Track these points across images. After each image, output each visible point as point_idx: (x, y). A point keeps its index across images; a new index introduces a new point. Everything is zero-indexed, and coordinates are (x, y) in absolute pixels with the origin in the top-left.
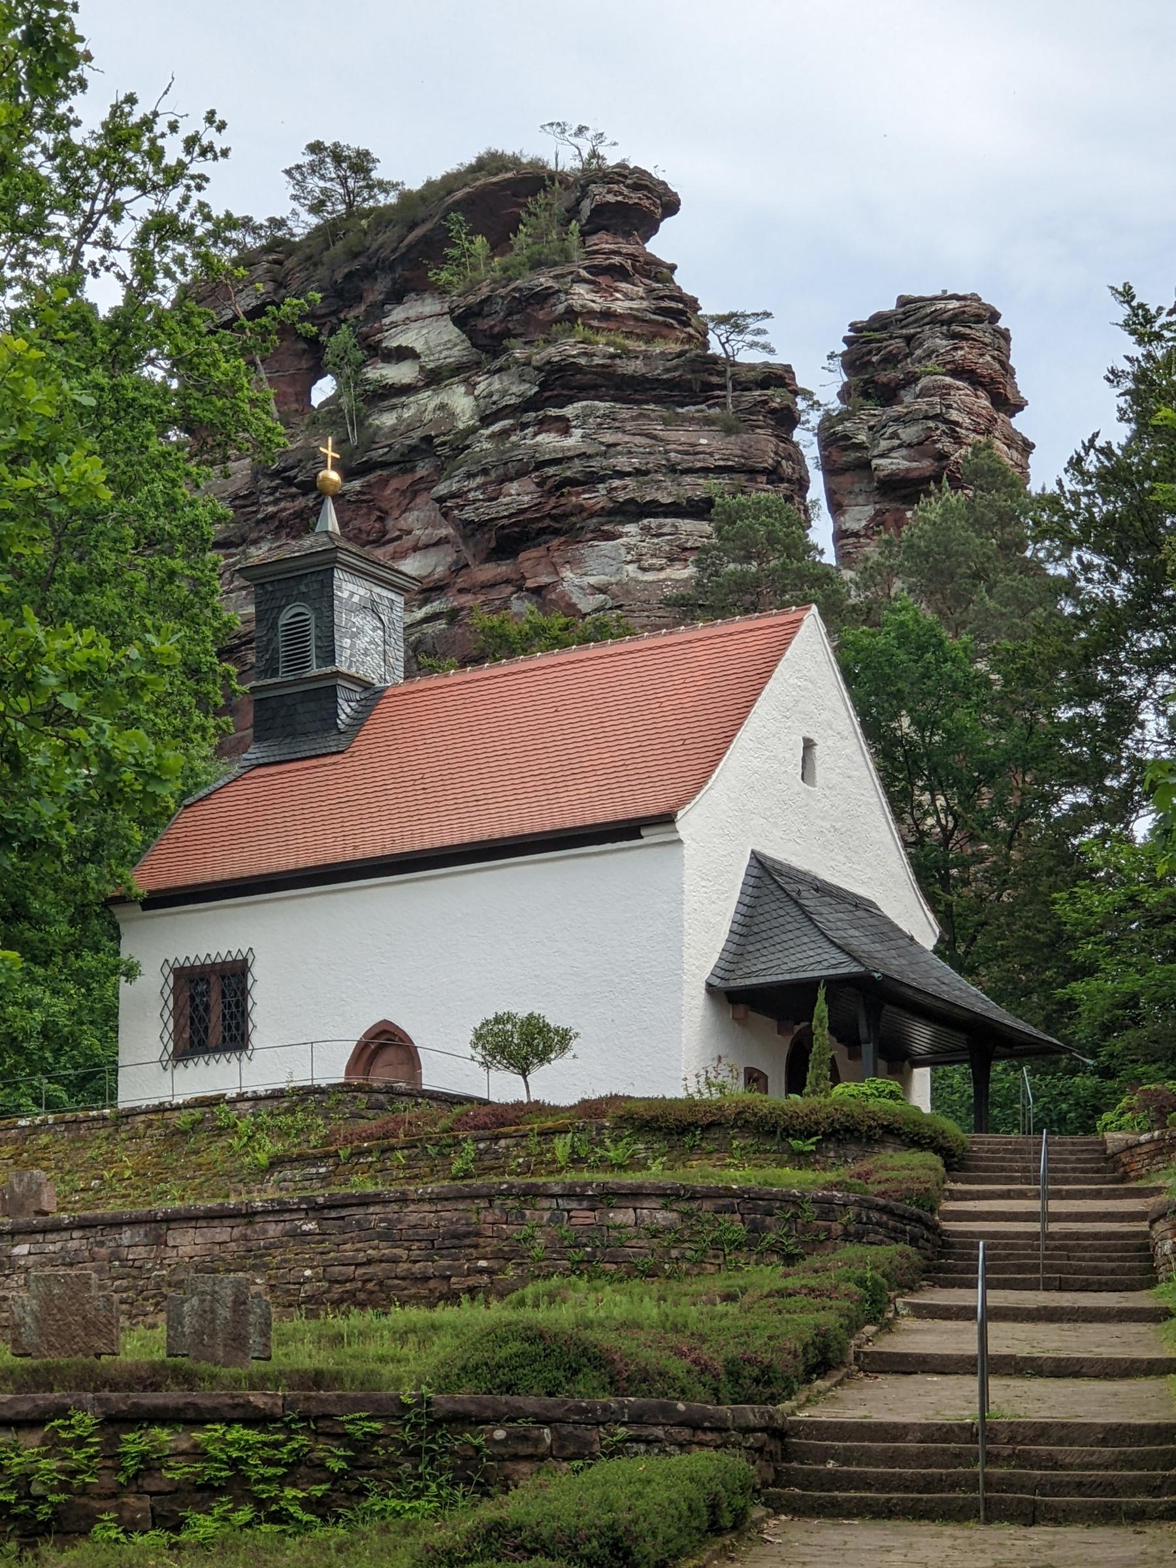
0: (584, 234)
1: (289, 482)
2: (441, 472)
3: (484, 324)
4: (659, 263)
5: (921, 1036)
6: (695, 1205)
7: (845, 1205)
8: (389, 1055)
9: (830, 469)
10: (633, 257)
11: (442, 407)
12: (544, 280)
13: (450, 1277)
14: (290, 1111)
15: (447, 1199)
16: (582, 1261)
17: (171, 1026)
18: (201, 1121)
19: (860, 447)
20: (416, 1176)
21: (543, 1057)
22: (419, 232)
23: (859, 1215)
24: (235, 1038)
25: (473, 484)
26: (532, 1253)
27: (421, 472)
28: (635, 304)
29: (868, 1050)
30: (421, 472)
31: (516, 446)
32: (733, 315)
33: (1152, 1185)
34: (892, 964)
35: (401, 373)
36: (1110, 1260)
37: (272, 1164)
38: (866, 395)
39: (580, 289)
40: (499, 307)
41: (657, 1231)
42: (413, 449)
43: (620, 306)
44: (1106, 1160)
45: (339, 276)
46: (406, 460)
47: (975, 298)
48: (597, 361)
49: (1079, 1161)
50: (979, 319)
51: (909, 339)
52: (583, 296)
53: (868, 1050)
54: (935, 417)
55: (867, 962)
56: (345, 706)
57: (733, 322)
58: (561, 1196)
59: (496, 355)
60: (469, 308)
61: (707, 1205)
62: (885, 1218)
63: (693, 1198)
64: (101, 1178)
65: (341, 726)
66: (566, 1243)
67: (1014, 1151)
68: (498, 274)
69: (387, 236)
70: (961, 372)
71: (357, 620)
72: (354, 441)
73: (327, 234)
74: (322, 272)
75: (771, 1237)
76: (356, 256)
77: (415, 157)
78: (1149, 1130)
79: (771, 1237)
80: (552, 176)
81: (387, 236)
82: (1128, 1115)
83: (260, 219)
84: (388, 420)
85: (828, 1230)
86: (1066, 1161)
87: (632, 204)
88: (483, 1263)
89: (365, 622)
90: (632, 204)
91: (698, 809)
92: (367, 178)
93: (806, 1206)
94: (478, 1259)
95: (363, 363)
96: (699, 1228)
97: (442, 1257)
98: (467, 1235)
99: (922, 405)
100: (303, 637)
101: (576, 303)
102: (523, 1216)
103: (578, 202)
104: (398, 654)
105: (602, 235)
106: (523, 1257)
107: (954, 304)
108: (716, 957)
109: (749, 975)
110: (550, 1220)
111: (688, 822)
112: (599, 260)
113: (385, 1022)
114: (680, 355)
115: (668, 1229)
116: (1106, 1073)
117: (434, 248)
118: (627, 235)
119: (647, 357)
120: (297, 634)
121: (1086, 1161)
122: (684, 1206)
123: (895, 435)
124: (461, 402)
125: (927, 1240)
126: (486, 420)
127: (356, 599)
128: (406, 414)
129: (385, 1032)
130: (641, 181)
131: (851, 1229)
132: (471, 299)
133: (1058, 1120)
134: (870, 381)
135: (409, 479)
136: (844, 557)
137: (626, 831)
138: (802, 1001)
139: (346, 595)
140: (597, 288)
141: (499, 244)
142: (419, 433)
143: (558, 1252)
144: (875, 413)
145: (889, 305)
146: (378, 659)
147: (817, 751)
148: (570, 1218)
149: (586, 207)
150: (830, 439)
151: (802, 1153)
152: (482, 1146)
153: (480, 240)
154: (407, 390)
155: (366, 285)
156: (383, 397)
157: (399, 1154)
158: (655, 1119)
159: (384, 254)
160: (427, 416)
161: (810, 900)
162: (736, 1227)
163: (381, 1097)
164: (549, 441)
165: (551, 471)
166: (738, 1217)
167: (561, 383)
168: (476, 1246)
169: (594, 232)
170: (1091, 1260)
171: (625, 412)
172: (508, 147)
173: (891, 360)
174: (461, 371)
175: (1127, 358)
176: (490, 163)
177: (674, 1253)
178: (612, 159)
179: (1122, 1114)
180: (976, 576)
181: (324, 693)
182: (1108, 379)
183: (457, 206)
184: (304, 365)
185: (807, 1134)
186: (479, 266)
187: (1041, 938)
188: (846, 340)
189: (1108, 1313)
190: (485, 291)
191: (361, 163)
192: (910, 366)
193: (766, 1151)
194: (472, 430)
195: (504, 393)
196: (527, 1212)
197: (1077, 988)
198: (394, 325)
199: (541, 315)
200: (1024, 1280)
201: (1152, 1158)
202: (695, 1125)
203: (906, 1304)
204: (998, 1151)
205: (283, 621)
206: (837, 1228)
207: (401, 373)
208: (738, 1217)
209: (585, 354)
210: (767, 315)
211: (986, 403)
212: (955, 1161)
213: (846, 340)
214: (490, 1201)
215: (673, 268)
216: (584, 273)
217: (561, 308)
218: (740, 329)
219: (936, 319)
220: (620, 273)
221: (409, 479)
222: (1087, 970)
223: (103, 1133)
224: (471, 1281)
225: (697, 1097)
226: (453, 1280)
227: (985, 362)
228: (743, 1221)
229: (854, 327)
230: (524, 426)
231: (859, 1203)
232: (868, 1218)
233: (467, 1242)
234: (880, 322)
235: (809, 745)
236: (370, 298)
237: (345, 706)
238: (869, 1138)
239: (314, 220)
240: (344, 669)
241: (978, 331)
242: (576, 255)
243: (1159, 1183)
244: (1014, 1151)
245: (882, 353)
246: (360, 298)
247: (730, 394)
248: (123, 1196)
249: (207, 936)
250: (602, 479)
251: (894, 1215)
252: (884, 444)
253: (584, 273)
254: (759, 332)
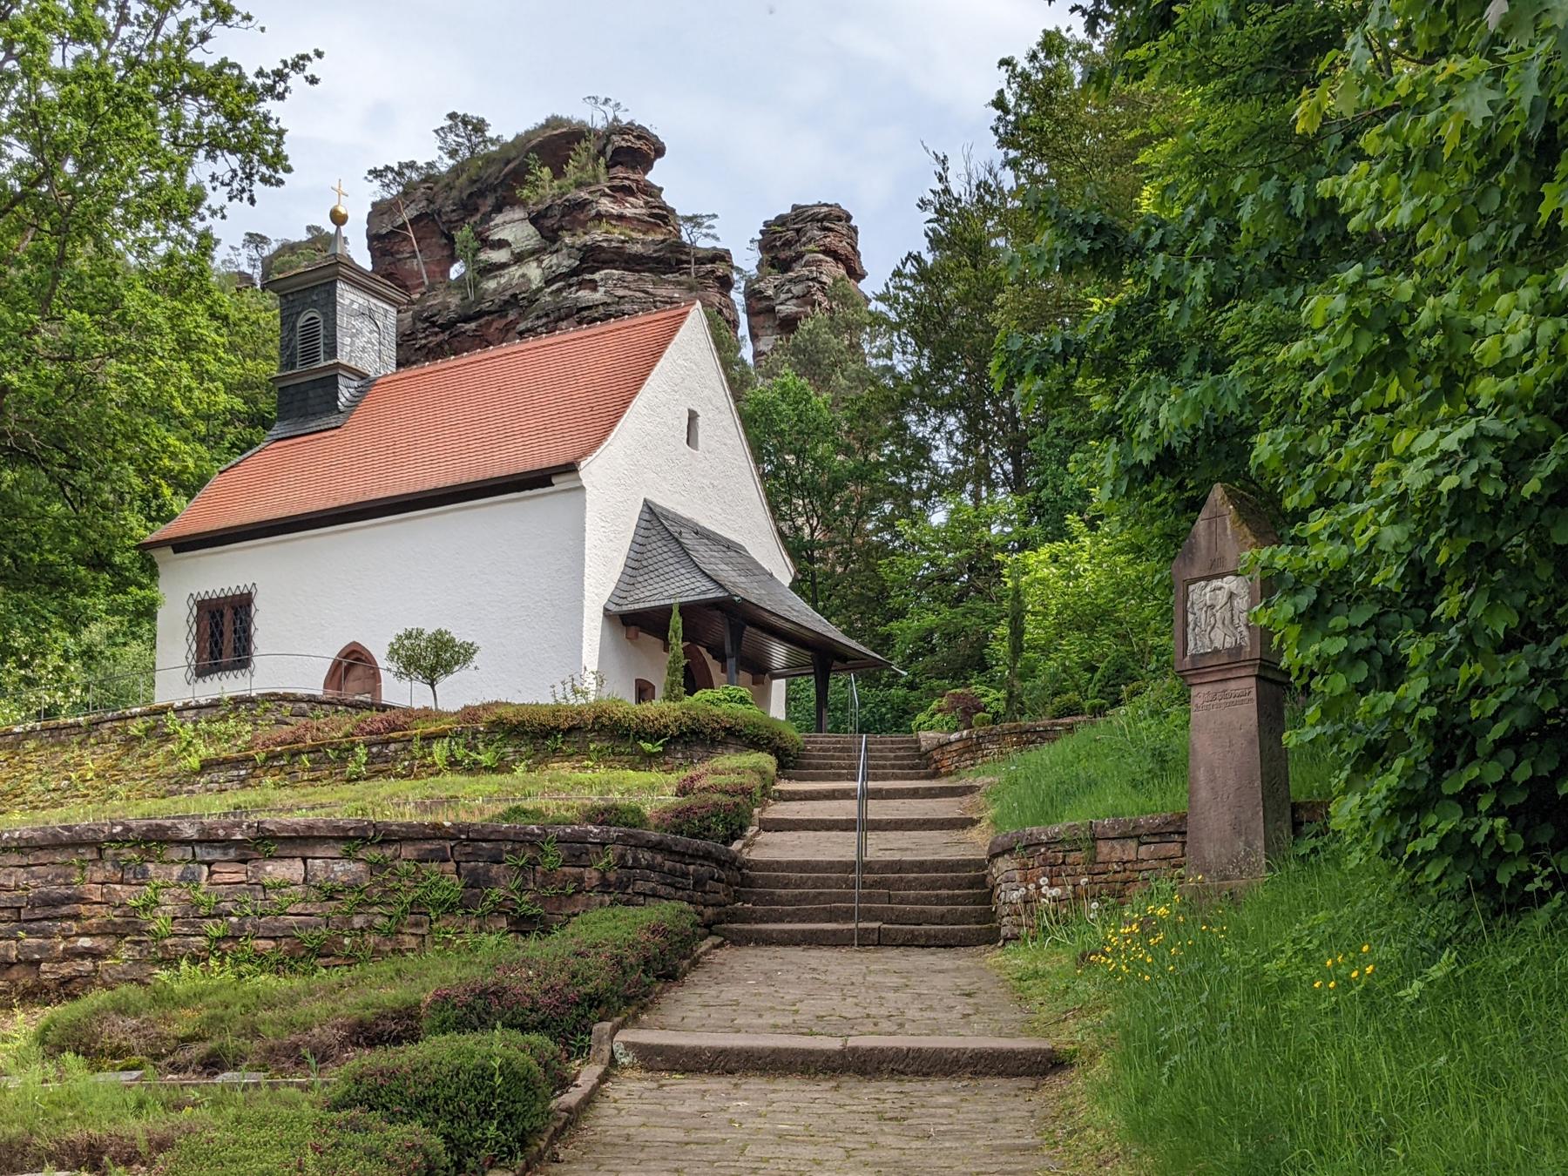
0: (608, 167)
1: (434, 324)
2: (523, 316)
3: (548, 223)
4: (653, 186)
5: (779, 654)
6: (389, 852)
7: (603, 845)
8: (358, 671)
9: (750, 313)
10: (637, 181)
11: (523, 276)
12: (584, 195)
13: (39, 962)
14: (224, 719)
15: (41, 848)
16: (224, 938)
17: (194, 647)
18: (154, 728)
19: (769, 298)
20: (317, 779)
21: (448, 668)
22: (511, 166)
23: (622, 856)
24: (241, 659)
25: (540, 323)
26: (153, 927)
27: (511, 317)
29: (731, 662)
30: (511, 317)
31: (566, 298)
32: (695, 217)
33: (961, 783)
35: (500, 256)
36: (940, 901)
37: (202, 767)
38: (773, 266)
39: (604, 200)
40: (557, 212)
41: (334, 890)
42: (506, 302)
44: (920, 757)
45: (464, 196)
46: (502, 310)
47: (837, 206)
49: (896, 758)
50: (839, 219)
51: (798, 231)
52: (606, 205)
53: (731, 662)
54: (813, 279)
55: (729, 586)
56: (345, 391)
57: (695, 220)
58: (199, 842)
59: (554, 242)
60: (539, 212)
61: (408, 851)
62: (659, 858)
63: (385, 842)
64: (69, 779)
65: (341, 408)
66: (202, 911)
67: (842, 750)
68: (556, 191)
69: (492, 169)
70: (828, 252)
71: (357, 323)
72: (472, 298)
73: (456, 171)
74: (455, 193)
75: (497, 893)
76: (475, 182)
77: (509, 123)
78: (956, 729)
79: (497, 893)
80: (589, 131)
81: (492, 169)
82: (939, 716)
83: (421, 163)
84: (491, 285)
85: (580, 880)
86: (885, 758)
87: (633, 151)
88: (85, 942)
89: (366, 326)
90: (633, 151)
91: (598, 461)
92: (483, 135)
93: (547, 848)
94: (78, 935)
95: (479, 250)
96: (395, 884)
97: (29, 933)
98: (66, 900)
99: (805, 271)
100: (315, 336)
101: (602, 208)
102: (145, 872)
103: (605, 146)
104: (391, 354)
105: (619, 168)
106: (140, 933)
107: (825, 209)
108: (613, 586)
109: (637, 601)
110: (182, 878)
111: (590, 471)
112: (617, 182)
113: (355, 643)
114: (663, 241)
115: (350, 887)
116: (912, 686)
117: (519, 175)
118: (634, 168)
119: (644, 243)
120: (310, 332)
121: (903, 758)
122: (373, 854)
123: (789, 291)
124: (534, 272)
125: (720, 880)
126: (548, 282)
127: (355, 306)
128: (503, 281)
129: (353, 652)
130: (642, 134)
131: (612, 876)
132: (540, 207)
135: (504, 322)
136: (757, 365)
137: (538, 479)
138: (693, 630)
139: (347, 302)
140: (615, 201)
141: (558, 173)
142: (510, 292)
143: (192, 925)
144: (775, 278)
145: (786, 210)
146: (374, 356)
147: (700, 421)
148: (211, 874)
149: (609, 149)
150: (752, 294)
151: (652, 755)
152: (374, 750)
153: (546, 170)
154: (504, 266)
155: (480, 201)
156: (490, 271)
157: (304, 757)
158: (522, 723)
159: (491, 180)
160: (514, 282)
161: (688, 540)
162: (447, 879)
163: (304, 705)
164: (585, 295)
166: (451, 866)
167: (592, 258)
168: (76, 917)
169: (614, 166)
170: (917, 901)
171: (629, 276)
172: (564, 114)
173: (788, 244)
174: (535, 253)
176: (554, 122)
177: (358, 921)
178: (625, 119)
179: (933, 715)
180: (834, 364)
181: (328, 384)
183: (533, 149)
184: (446, 253)
185: (654, 737)
186: (545, 187)
187: (871, 594)
188: (762, 232)
189: (956, 1060)
190: (549, 202)
191: (479, 127)
193: (622, 753)
194: (540, 290)
195: (559, 266)
196: (151, 866)
198: (497, 226)
199: (582, 217)
200: (834, 932)
201: (961, 755)
202: (556, 729)
203: (629, 1046)
204: (828, 750)
205: (300, 324)
206: (591, 876)
207: (500, 256)
208: (451, 866)
211: (843, 272)
212: (790, 762)
213: (762, 232)
214: (100, 851)
215: (661, 189)
217: (593, 212)
218: (699, 225)
219: (814, 218)
220: (628, 191)
221: (504, 322)
222: (900, 614)
223: (76, 739)
224: (66, 970)
225: (564, 702)
226: (44, 967)
227: (843, 247)
228: (458, 873)
229: (766, 224)
230: (571, 286)
231: (623, 840)
232: (635, 859)
233: (64, 910)
234: (781, 220)
235: (693, 416)
236: (483, 209)
237: (345, 391)
238: (713, 740)
239: (451, 162)
240: (344, 362)
242: (603, 178)
243: (970, 781)
244: (842, 750)
246: (477, 210)
247: (693, 267)
248: (85, 796)
249: (218, 575)
251: (671, 852)
252: (783, 296)
254: (710, 227)
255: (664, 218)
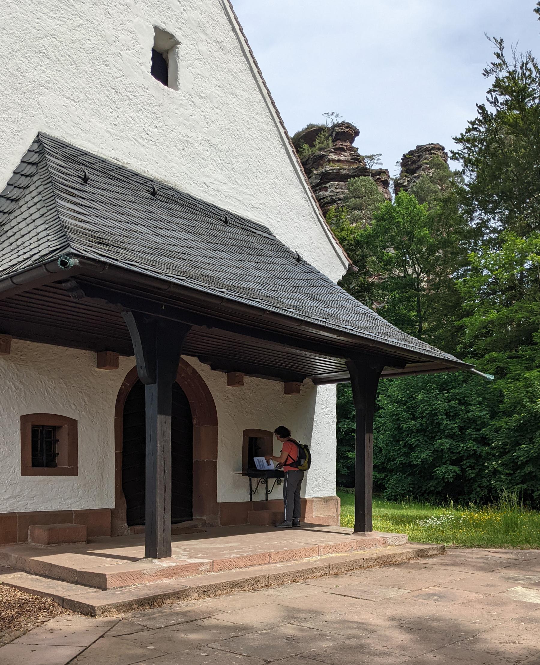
28: (346, 158)
34: (288, 301)
43: (342, 158)
48: (335, 171)
50: (439, 149)
51: (419, 156)
52: (332, 156)
57: (371, 158)
101: (330, 157)
114: (357, 168)
130: (349, 126)
133: (455, 380)
134: (408, 169)
140: (336, 154)
149: (334, 134)
165: (322, 201)
173: (414, 162)
175: (492, 63)
176: (311, 126)
182: (485, 75)
188: (402, 159)
192: (419, 163)
197: (466, 320)
209: (332, 170)
210: (381, 155)
213: (402, 159)
215: (358, 149)
216: (332, 150)
217: (327, 160)
234: (411, 153)
241: (439, 153)
245: (411, 162)
250: (335, 202)
253: (332, 150)
254: (378, 159)
255: (357, 160)
